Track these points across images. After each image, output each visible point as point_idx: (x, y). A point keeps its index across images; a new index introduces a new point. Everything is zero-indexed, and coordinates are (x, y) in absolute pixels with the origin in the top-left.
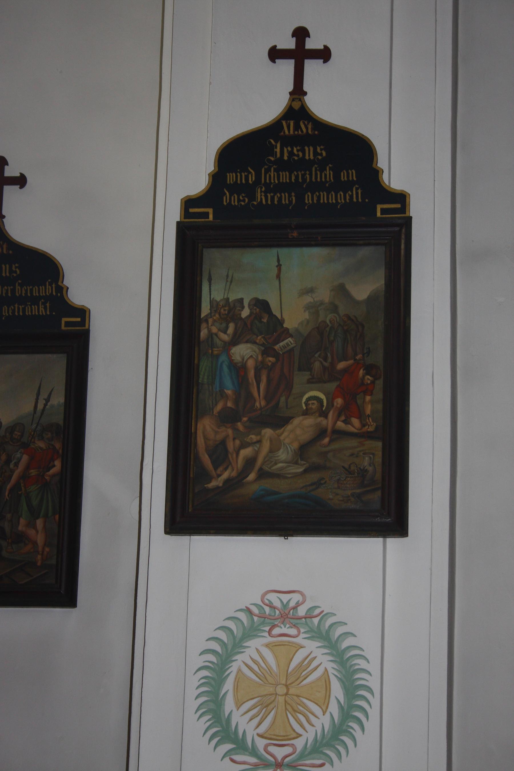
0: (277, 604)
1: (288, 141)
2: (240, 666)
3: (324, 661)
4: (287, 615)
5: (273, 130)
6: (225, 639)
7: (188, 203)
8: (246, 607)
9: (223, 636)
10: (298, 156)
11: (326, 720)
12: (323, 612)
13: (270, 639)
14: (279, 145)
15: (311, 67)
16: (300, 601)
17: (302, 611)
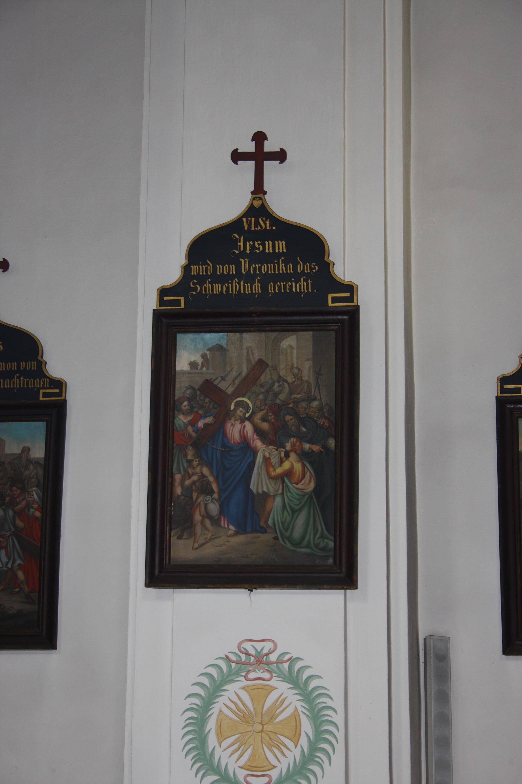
0: (252, 651)
1: (250, 236)
2: (220, 709)
3: (294, 701)
4: (260, 660)
5: (235, 226)
6: (215, 675)
7: (163, 292)
8: (226, 656)
9: (205, 681)
10: (259, 249)
11: (297, 753)
12: (292, 657)
13: (246, 683)
14: (242, 238)
15: (269, 165)
16: (272, 649)
17: (273, 657)
